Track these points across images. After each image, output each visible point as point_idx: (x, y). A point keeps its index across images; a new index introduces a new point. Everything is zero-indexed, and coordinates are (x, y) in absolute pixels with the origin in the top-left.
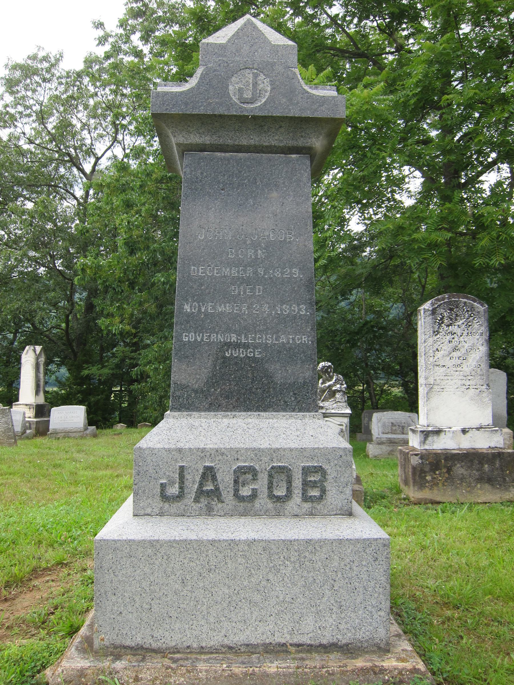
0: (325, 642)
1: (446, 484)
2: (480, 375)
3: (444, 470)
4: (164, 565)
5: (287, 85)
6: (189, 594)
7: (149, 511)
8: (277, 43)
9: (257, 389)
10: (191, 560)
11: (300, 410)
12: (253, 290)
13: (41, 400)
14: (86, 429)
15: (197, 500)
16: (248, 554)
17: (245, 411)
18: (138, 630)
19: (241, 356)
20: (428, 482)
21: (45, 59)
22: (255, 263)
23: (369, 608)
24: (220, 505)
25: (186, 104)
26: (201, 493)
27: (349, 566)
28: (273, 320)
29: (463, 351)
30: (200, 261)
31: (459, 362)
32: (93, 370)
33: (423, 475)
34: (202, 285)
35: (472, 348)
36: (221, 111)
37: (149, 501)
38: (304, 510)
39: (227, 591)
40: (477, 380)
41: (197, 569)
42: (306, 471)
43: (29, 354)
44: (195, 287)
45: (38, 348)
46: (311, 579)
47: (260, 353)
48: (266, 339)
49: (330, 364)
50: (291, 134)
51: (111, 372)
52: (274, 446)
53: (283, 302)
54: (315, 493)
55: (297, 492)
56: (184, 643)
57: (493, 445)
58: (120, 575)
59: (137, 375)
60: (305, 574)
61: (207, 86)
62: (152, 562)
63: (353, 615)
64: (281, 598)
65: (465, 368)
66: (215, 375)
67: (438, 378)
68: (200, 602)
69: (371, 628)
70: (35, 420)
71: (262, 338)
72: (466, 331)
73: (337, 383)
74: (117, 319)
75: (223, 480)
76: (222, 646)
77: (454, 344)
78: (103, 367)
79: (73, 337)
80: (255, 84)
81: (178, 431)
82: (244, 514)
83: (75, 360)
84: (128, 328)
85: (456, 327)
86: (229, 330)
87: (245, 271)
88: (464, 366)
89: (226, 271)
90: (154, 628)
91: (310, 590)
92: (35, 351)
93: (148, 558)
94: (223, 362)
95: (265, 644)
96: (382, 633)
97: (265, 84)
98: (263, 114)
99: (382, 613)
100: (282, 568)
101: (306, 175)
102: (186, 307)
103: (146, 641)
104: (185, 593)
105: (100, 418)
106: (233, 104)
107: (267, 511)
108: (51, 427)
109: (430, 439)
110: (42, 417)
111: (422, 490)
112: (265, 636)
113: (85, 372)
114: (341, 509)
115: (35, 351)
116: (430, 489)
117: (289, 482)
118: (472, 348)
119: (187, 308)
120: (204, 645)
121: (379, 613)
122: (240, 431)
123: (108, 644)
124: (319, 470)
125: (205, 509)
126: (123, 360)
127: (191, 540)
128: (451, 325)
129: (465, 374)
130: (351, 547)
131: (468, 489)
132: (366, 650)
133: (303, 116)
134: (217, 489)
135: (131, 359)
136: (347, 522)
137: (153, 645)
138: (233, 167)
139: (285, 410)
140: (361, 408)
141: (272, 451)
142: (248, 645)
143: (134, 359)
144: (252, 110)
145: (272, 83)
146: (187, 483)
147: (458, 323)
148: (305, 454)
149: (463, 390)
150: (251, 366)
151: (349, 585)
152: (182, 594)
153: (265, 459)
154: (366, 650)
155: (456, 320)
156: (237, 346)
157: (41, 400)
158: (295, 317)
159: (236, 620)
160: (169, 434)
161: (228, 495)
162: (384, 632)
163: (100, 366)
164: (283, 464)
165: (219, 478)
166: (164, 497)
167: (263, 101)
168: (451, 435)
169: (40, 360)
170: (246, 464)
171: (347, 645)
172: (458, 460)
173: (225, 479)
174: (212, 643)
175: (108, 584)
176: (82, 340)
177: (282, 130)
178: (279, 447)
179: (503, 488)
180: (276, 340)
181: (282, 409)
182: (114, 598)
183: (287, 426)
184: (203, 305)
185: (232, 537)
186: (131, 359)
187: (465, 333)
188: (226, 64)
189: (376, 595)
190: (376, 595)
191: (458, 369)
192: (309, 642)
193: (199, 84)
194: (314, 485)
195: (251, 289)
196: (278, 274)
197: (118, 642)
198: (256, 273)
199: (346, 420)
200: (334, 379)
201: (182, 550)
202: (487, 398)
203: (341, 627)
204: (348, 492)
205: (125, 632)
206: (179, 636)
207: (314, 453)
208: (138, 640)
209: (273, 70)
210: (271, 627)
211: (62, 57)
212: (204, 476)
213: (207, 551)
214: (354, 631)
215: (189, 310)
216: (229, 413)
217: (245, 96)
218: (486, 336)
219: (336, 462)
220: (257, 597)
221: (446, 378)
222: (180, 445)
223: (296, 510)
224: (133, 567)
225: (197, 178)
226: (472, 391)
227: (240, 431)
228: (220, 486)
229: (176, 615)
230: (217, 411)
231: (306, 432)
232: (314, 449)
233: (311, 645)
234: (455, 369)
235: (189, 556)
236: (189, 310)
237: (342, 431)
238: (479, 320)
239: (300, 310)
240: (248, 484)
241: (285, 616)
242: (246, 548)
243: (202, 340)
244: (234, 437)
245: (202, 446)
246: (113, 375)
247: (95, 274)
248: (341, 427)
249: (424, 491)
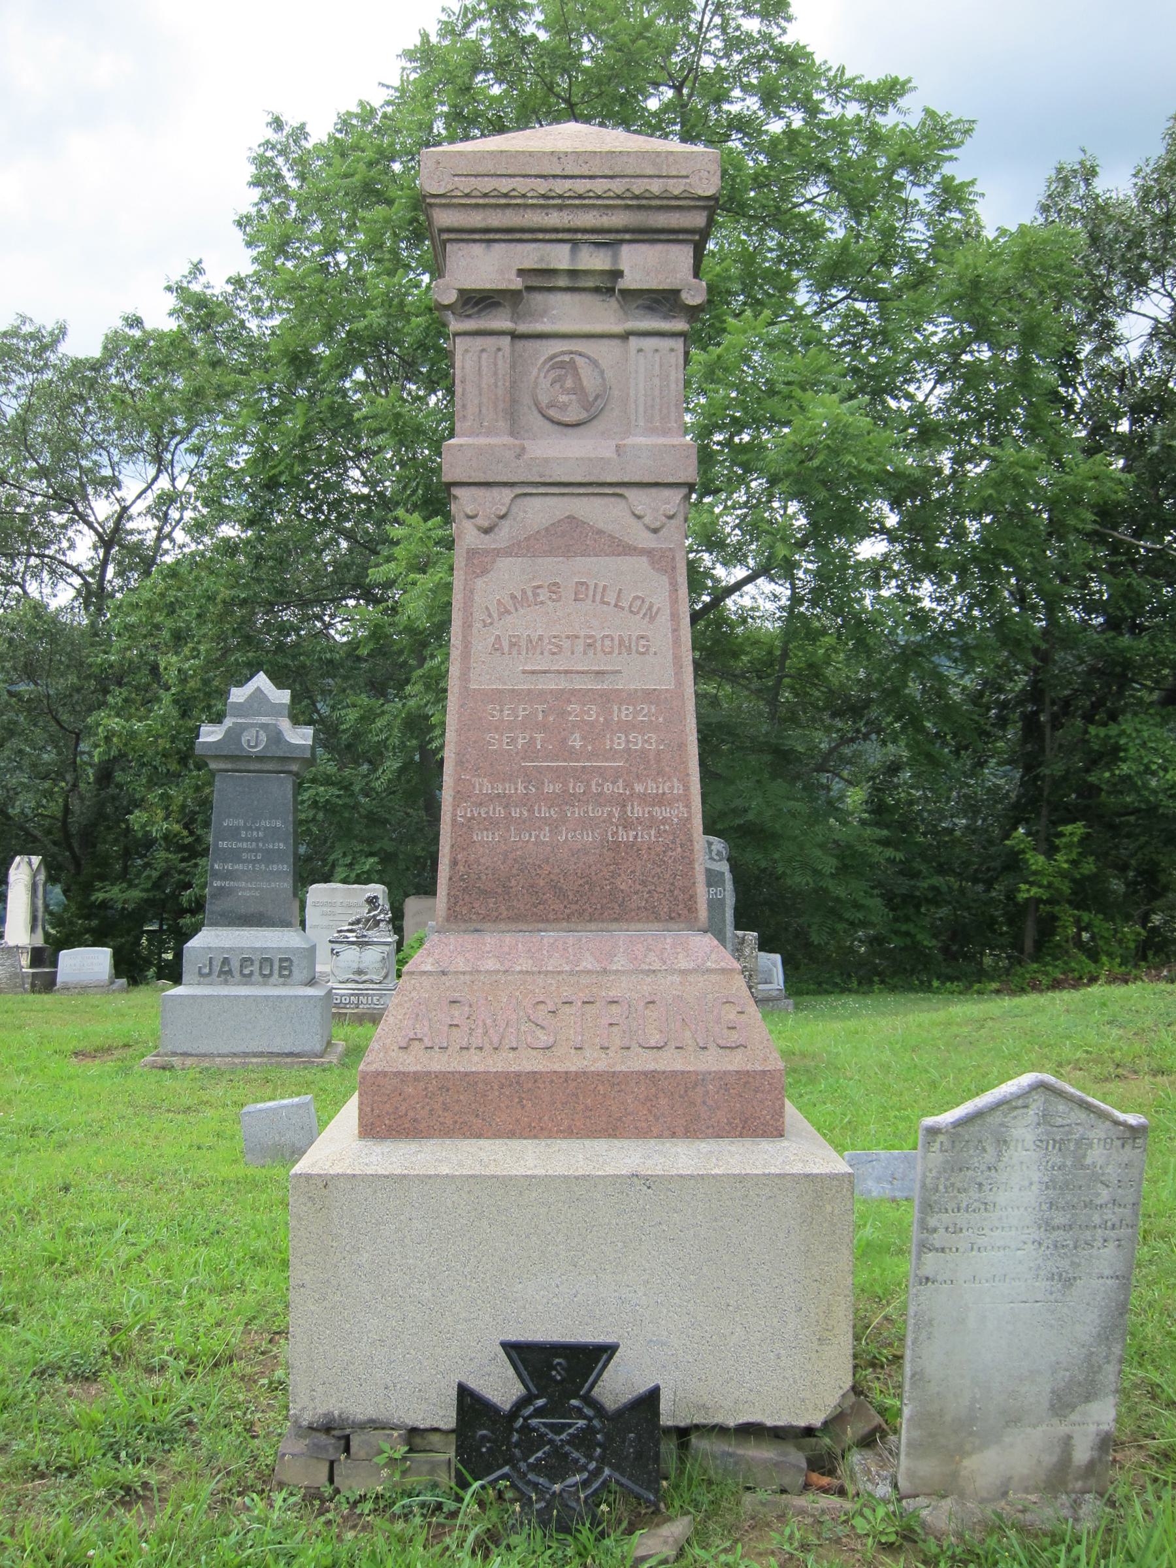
13: (39, 941)
14: (112, 983)
21: (33, 336)
22: (257, 840)
26: (221, 973)
32: (114, 893)
42: (281, 960)
45: (36, 860)
51: (144, 895)
55: (276, 972)
59: (190, 901)
74: (161, 813)
78: (131, 885)
79: (73, 830)
83: (78, 873)
84: (177, 827)
92: (30, 863)
97: (263, 737)
105: (131, 969)
108: (59, 979)
113: (100, 896)
115: (30, 863)
124: (287, 960)
126: (166, 874)
135: (180, 872)
143: (187, 874)
157: (39, 941)
161: (236, 973)
163: (124, 885)
166: (201, 974)
173: (235, 964)
176: (89, 836)
186: (180, 872)
194: (285, 968)
207: (286, 950)
211: (64, 334)
246: (147, 901)
247: (126, 745)
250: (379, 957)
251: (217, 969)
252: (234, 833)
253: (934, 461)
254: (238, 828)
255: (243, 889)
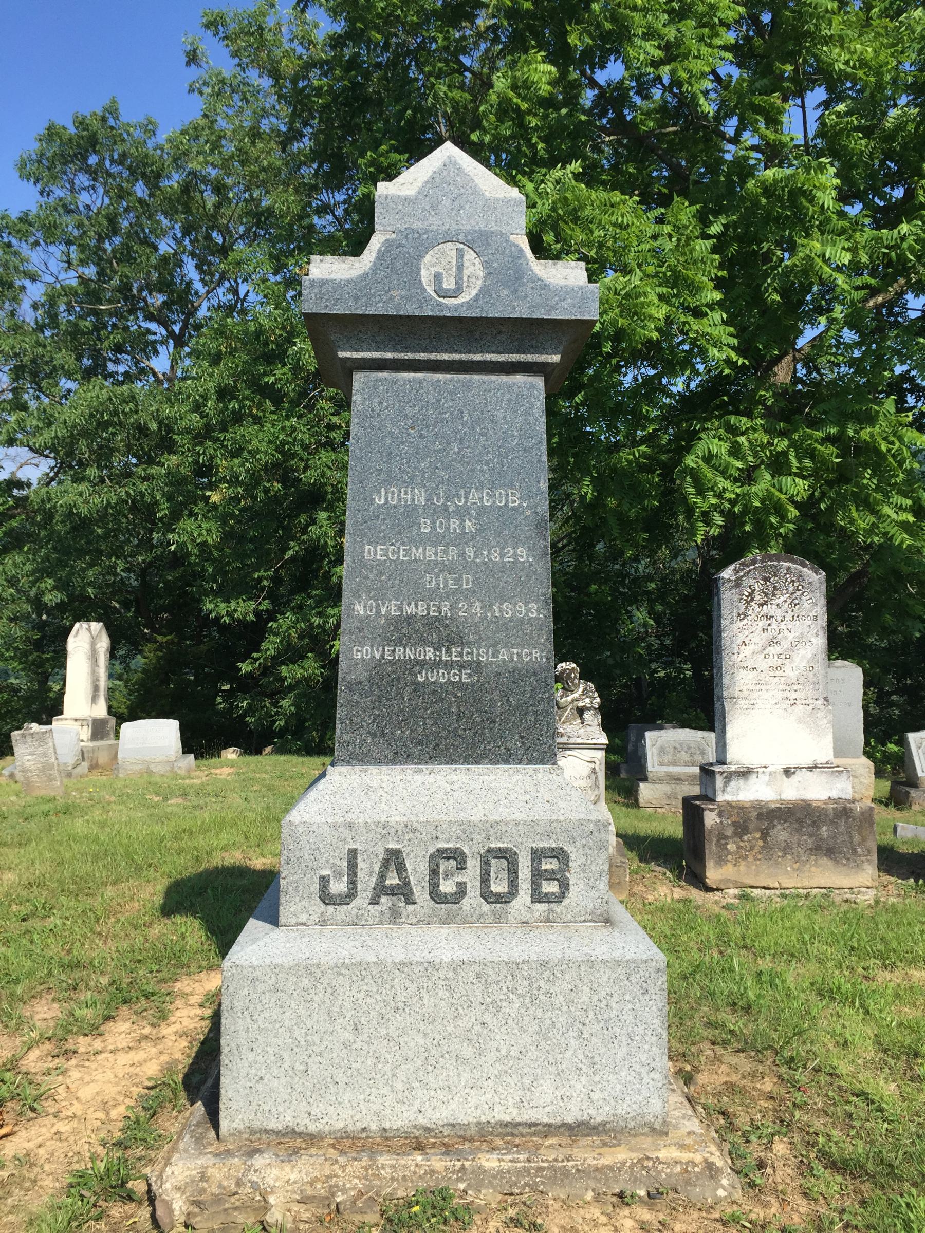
0: (570, 1120)
1: (760, 857)
2: (814, 683)
3: (758, 835)
4: (328, 1001)
5: (509, 268)
6: (365, 1047)
7: (303, 918)
8: (494, 195)
9: (465, 730)
10: (368, 995)
11: (530, 762)
12: (458, 581)
15: (374, 902)
16: (453, 984)
17: (447, 763)
18: (287, 1104)
19: (442, 680)
20: (731, 854)
22: (462, 539)
23: (637, 1067)
24: (411, 908)
25: (356, 299)
26: (381, 890)
27: (604, 1002)
28: (489, 626)
29: (786, 644)
30: (378, 538)
31: (779, 662)
33: (723, 842)
34: (381, 574)
35: (800, 641)
36: (411, 309)
37: (303, 903)
38: (537, 915)
39: (421, 1042)
40: (808, 691)
41: (377, 1008)
42: (537, 855)
43: (80, 636)
44: (371, 576)
46: (549, 1022)
47: (470, 676)
48: (478, 655)
49: (574, 665)
50: (516, 343)
52: (491, 818)
53: (502, 599)
54: (550, 887)
55: (525, 886)
56: (358, 1124)
57: (835, 794)
58: (261, 1019)
60: (539, 1014)
61: (388, 271)
62: (309, 998)
63: (612, 1078)
64: (504, 1052)
65: (789, 672)
66: (402, 710)
67: (745, 688)
68: (382, 1060)
69: (641, 1099)
70: (91, 744)
71: (472, 653)
72: (791, 614)
73: (584, 694)
75: (414, 870)
76: (415, 1127)
77: (770, 634)
80: (460, 268)
81: (347, 795)
82: (446, 921)
85: (774, 607)
86: (423, 642)
87: (445, 552)
88: (788, 668)
89: (418, 553)
90: (311, 1101)
91: (546, 1039)
92: (89, 630)
93: (303, 993)
94: (415, 690)
95: (479, 1123)
96: (656, 1106)
97: (474, 266)
98: (474, 315)
99: (657, 1076)
100: (504, 1004)
101: (539, 404)
102: (357, 607)
103: (299, 1120)
104: (359, 1045)
106: (428, 299)
107: (481, 916)
109: (733, 784)
110: (102, 739)
111: (721, 866)
112: (479, 1111)
114: (592, 913)
115: (89, 630)
116: (735, 865)
117: (513, 872)
118: (800, 641)
119: (359, 609)
120: (387, 1126)
121: (652, 1075)
122: (440, 795)
123: (241, 1127)
124: (560, 855)
125: (388, 914)
127: (368, 964)
128: (766, 603)
129: (789, 682)
130: (608, 972)
131: (796, 866)
132: (633, 1132)
133: (535, 316)
134: (407, 884)
136: (603, 933)
137: (310, 1128)
138: (428, 392)
139: (506, 762)
140: (625, 723)
141: (488, 825)
142: (453, 1125)
144: (457, 307)
145: (486, 265)
146: (360, 875)
147: (778, 601)
148: (539, 829)
149: (785, 706)
150: (456, 696)
151: (605, 1032)
152: (354, 1046)
153: (479, 838)
154: (633, 1132)
155: (774, 595)
156: (436, 665)
158: (521, 621)
159: (436, 1086)
160: (333, 800)
161: (421, 892)
162: (660, 1104)
164: (505, 845)
165: (409, 868)
166: (326, 898)
167: (474, 292)
168: (767, 778)
169: (98, 646)
170: (450, 845)
171: (604, 1124)
172: (779, 818)
173: (417, 868)
174: (399, 1123)
175: (243, 1034)
177: (503, 337)
178: (499, 819)
179: (853, 864)
180: (493, 656)
181: (503, 760)
182: (251, 1056)
183: (511, 786)
184: (384, 604)
185: (429, 957)
187: (789, 617)
188: (416, 235)
189: (647, 1047)
190: (647, 1047)
191: (778, 673)
192: (546, 1120)
193: (375, 269)
194: (551, 876)
195: (455, 579)
196: (495, 556)
197: (257, 1125)
198: (462, 555)
199: (600, 755)
200: (581, 689)
201: (355, 978)
202: (824, 720)
203: (594, 1096)
204: (602, 886)
205: (267, 1109)
206: (350, 1112)
208: (287, 1120)
209: (489, 244)
210: (489, 1096)
212: (386, 864)
213: (392, 980)
214: (613, 1103)
215: (362, 612)
216: (424, 767)
217: (445, 285)
218: (823, 621)
219: (584, 841)
220: (468, 1051)
221: (758, 687)
222: (350, 817)
223: (525, 915)
224: (281, 1007)
225: (373, 410)
226: (799, 709)
227: (440, 795)
228: (411, 878)
229: (345, 1080)
230: (406, 763)
231: (539, 795)
232: (551, 822)
233: (549, 1125)
234: (772, 674)
235: (365, 988)
236: (362, 612)
237: (594, 771)
238: (811, 595)
239: (529, 610)
240: (452, 875)
241: (509, 1080)
242: (451, 974)
243: (383, 657)
244: (431, 804)
245: (384, 819)
248: (592, 765)
249: (725, 868)
250: (586, 769)
251: (367, 880)
252: (402, 523)
253: (136, 671)
254: (411, 512)
255: (436, 665)
